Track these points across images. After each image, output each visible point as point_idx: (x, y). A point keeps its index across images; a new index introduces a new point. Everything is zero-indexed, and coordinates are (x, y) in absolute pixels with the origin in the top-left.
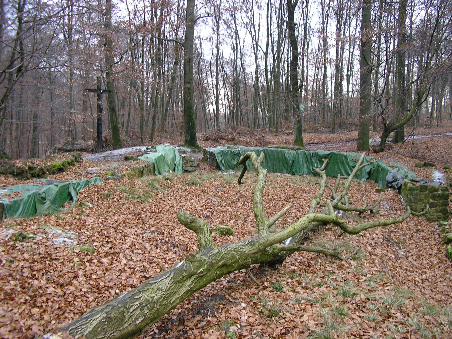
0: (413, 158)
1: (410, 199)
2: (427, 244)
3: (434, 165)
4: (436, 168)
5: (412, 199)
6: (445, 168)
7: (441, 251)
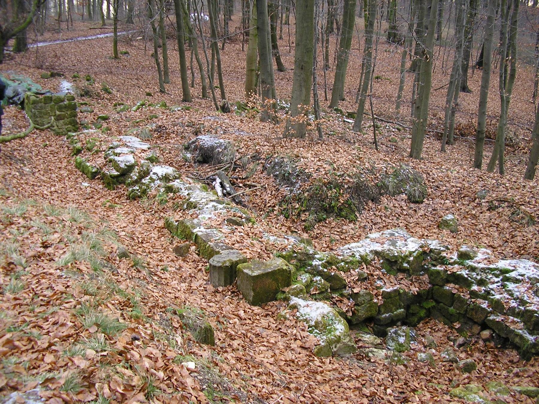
0: (38, 68)
1: (35, 114)
2: (56, 158)
3: (63, 75)
4: (65, 78)
5: (37, 113)
6: (75, 77)
7: (70, 163)
